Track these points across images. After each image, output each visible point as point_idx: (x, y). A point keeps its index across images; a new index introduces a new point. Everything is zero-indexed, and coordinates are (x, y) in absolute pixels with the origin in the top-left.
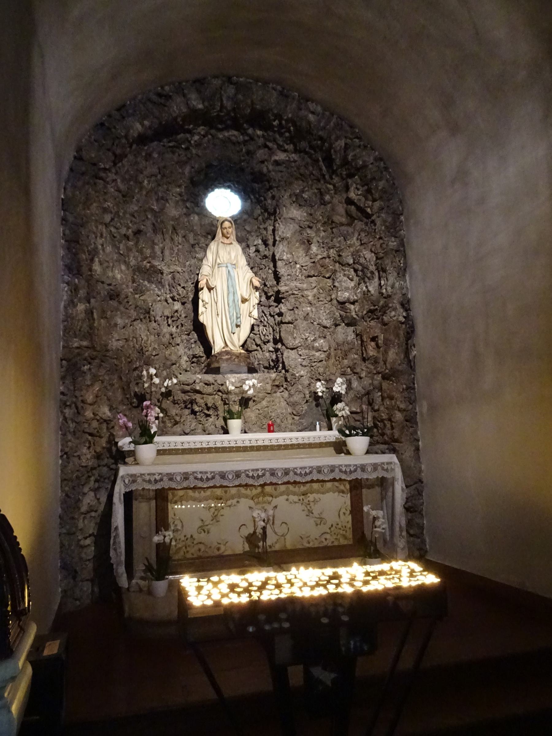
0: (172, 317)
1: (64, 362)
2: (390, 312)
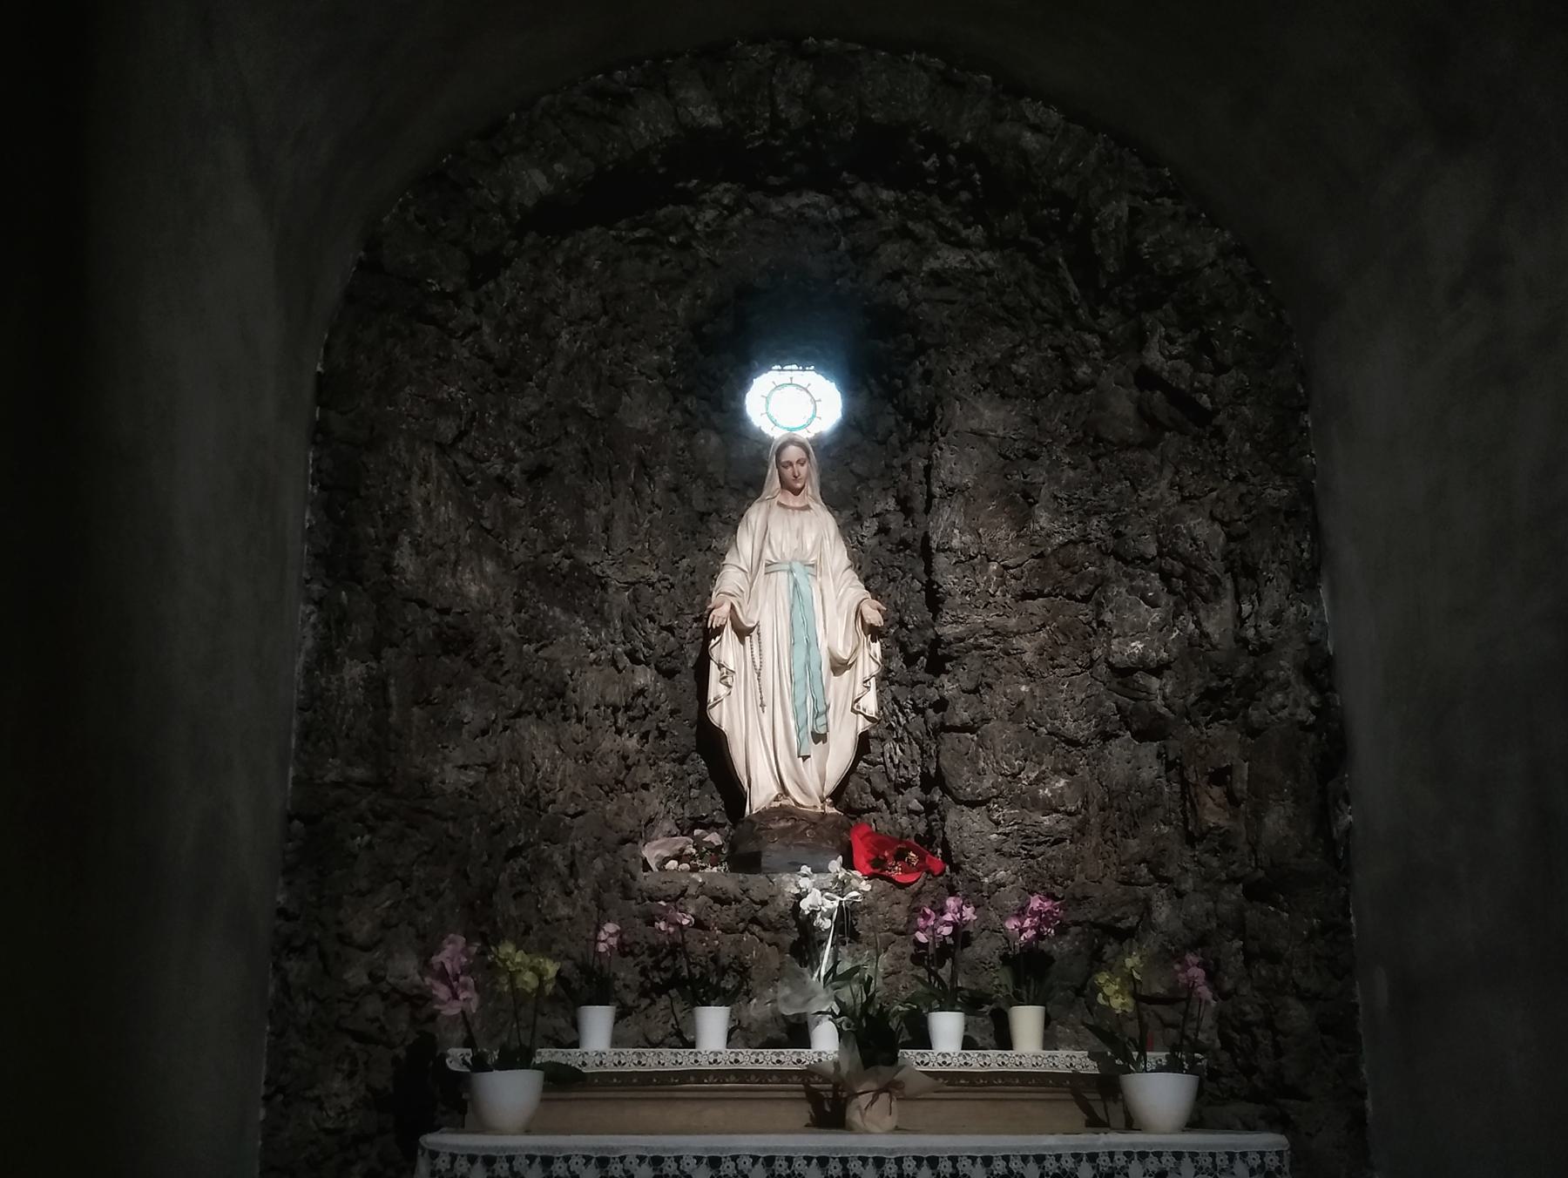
0: (628, 708)
1: (296, 823)
2: (1271, 694)
